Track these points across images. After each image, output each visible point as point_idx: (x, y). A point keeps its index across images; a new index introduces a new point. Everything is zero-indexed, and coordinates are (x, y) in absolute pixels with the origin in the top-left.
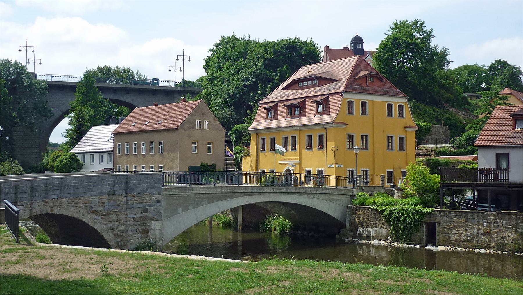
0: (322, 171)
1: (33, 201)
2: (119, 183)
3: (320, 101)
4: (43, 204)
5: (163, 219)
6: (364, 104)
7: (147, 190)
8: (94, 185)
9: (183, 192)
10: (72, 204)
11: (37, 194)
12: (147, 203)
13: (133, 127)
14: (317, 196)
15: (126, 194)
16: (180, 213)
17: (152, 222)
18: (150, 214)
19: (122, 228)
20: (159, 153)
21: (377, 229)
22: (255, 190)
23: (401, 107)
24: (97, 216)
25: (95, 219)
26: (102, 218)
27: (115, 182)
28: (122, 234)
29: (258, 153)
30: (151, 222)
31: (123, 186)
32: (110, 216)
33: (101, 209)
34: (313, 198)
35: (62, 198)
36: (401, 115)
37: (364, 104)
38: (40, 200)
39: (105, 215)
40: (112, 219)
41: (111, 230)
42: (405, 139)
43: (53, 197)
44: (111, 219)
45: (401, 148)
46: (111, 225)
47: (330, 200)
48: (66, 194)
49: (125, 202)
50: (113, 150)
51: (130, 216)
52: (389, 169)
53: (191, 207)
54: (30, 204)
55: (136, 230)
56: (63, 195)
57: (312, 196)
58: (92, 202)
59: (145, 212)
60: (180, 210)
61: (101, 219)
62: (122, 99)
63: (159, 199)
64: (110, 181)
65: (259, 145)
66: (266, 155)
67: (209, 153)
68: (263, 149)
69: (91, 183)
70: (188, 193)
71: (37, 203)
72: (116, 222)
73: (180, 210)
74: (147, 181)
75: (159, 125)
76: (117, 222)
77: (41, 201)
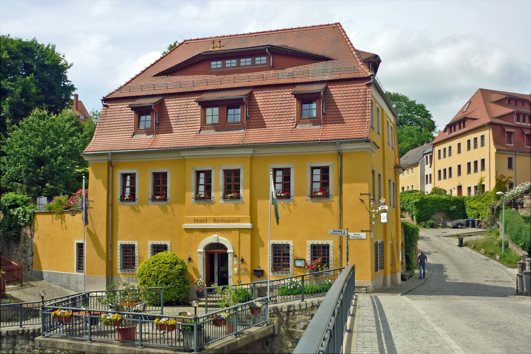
0: (133, 247)
3: (151, 106)
29: (112, 206)
66: (139, 211)
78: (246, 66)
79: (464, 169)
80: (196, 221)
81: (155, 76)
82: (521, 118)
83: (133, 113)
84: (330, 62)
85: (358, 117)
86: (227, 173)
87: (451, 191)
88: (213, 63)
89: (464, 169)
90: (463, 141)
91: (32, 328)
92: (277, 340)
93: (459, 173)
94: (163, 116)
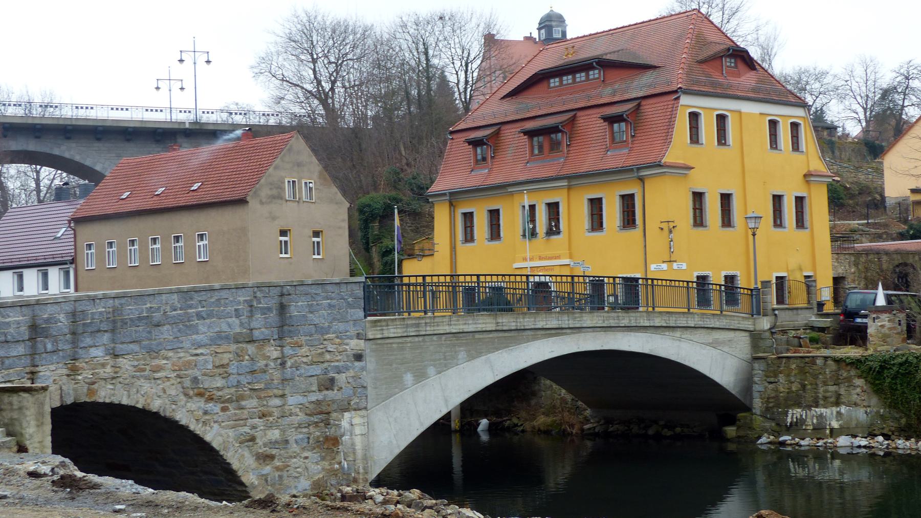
1: (37, 366)
2: (261, 308)
4: (68, 375)
5: (369, 407)
6: (721, 119)
7: (329, 327)
8: (199, 316)
9: (414, 329)
10: (146, 373)
11: (49, 347)
12: (332, 364)
13: (123, 202)
14: (687, 335)
15: (281, 338)
16: (408, 388)
17: (346, 414)
18: (339, 394)
19: (275, 434)
20: (198, 260)
21: (843, 409)
22: (567, 322)
23: (795, 126)
24: (211, 405)
25: (206, 413)
26: (224, 409)
27: (251, 306)
28: (273, 453)
30: (343, 415)
31: (273, 316)
32: (243, 403)
33: (219, 383)
34: (680, 341)
35: (116, 356)
36: (796, 146)
37: (721, 119)
38: (58, 363)
39: (229, 401)
40: (249, 412)
41: (246, 444)
42: (807, 203)
43: (94, 352)
44: (246, 412)
45: (800, 223)
46: (247, 429)
47: (712, 343)
48: (127, 343)
49: (279, 361)
50: (73, 259)
51: (293, 400)
52: (777, 272)
53: (431, 370)
54: (29, 376)
55: (309, 438)
56: (121, 346)
57: (678, 334)
58: (196, 365)
59: (327, 389)
60: (409, 378)
61: (219, 411)
62: (56, 152)
63: (360, 352)
64: (239, 303)
65: (456, 230)
67: (316, 257)
68: (469, 237)
69: (193, 308)
70: (424, 333)
71: (48, 373)
72: (258, 420)
73: (409, 378)
74: (328, 301)
75: (193, 194)
76: (261, 420)
77: (60, 365)
81: (502, 98)
83: (606, 123)
84: (657, 70)
86: (549, 205)
88: (552, 81)
94: (499, 148)
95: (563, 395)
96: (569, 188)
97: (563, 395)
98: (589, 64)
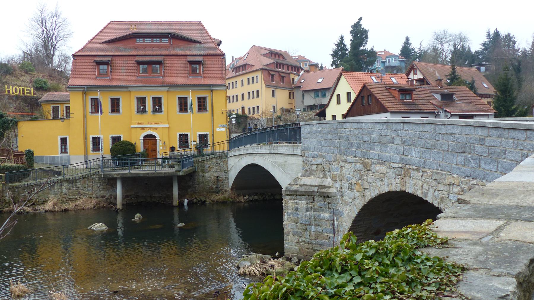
78: (157, 43)
79: (246, 96)
80: (138, 124)
82: (279, 65)
85: (219, 74)
86: (154, 99)
87: (237, 110)
88: (137, 39)
89: (246, 96)
90: (245, 78)
91: (71, 177)
92: (197, 174)
93: (243, 99)
95: (210, 186)
96: (168, 91)
97: (210, 186)
98: (167, 35)
